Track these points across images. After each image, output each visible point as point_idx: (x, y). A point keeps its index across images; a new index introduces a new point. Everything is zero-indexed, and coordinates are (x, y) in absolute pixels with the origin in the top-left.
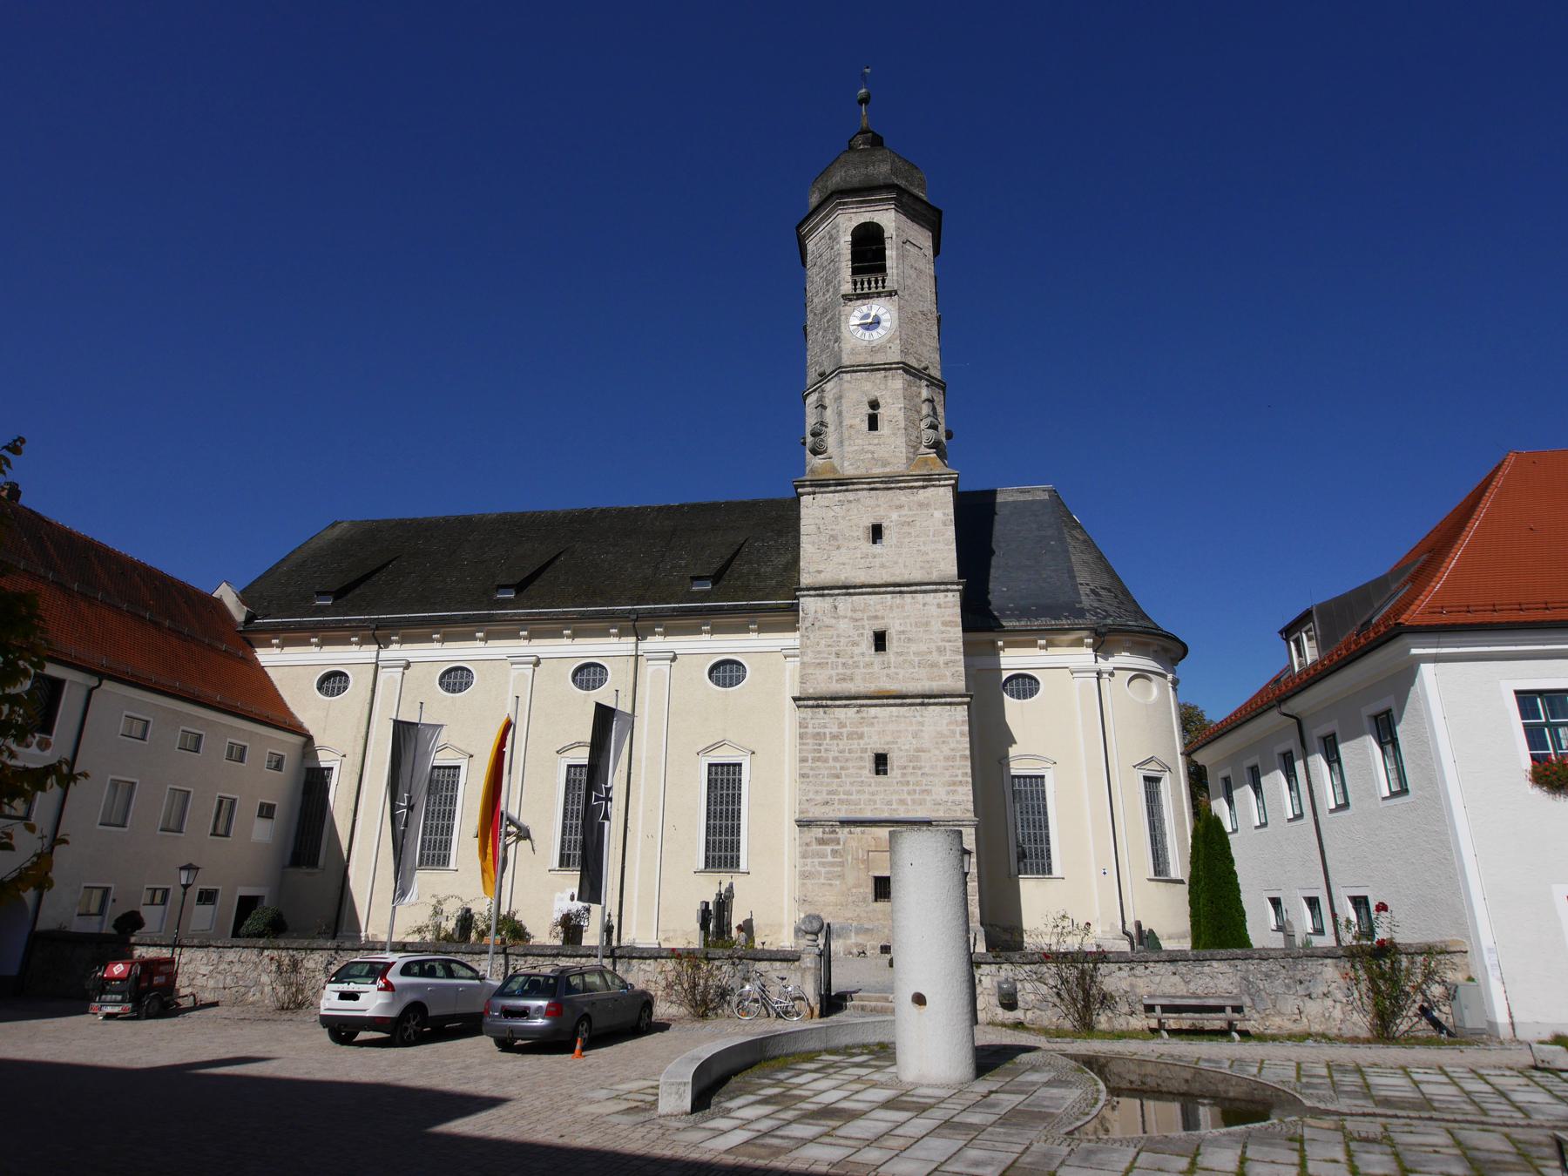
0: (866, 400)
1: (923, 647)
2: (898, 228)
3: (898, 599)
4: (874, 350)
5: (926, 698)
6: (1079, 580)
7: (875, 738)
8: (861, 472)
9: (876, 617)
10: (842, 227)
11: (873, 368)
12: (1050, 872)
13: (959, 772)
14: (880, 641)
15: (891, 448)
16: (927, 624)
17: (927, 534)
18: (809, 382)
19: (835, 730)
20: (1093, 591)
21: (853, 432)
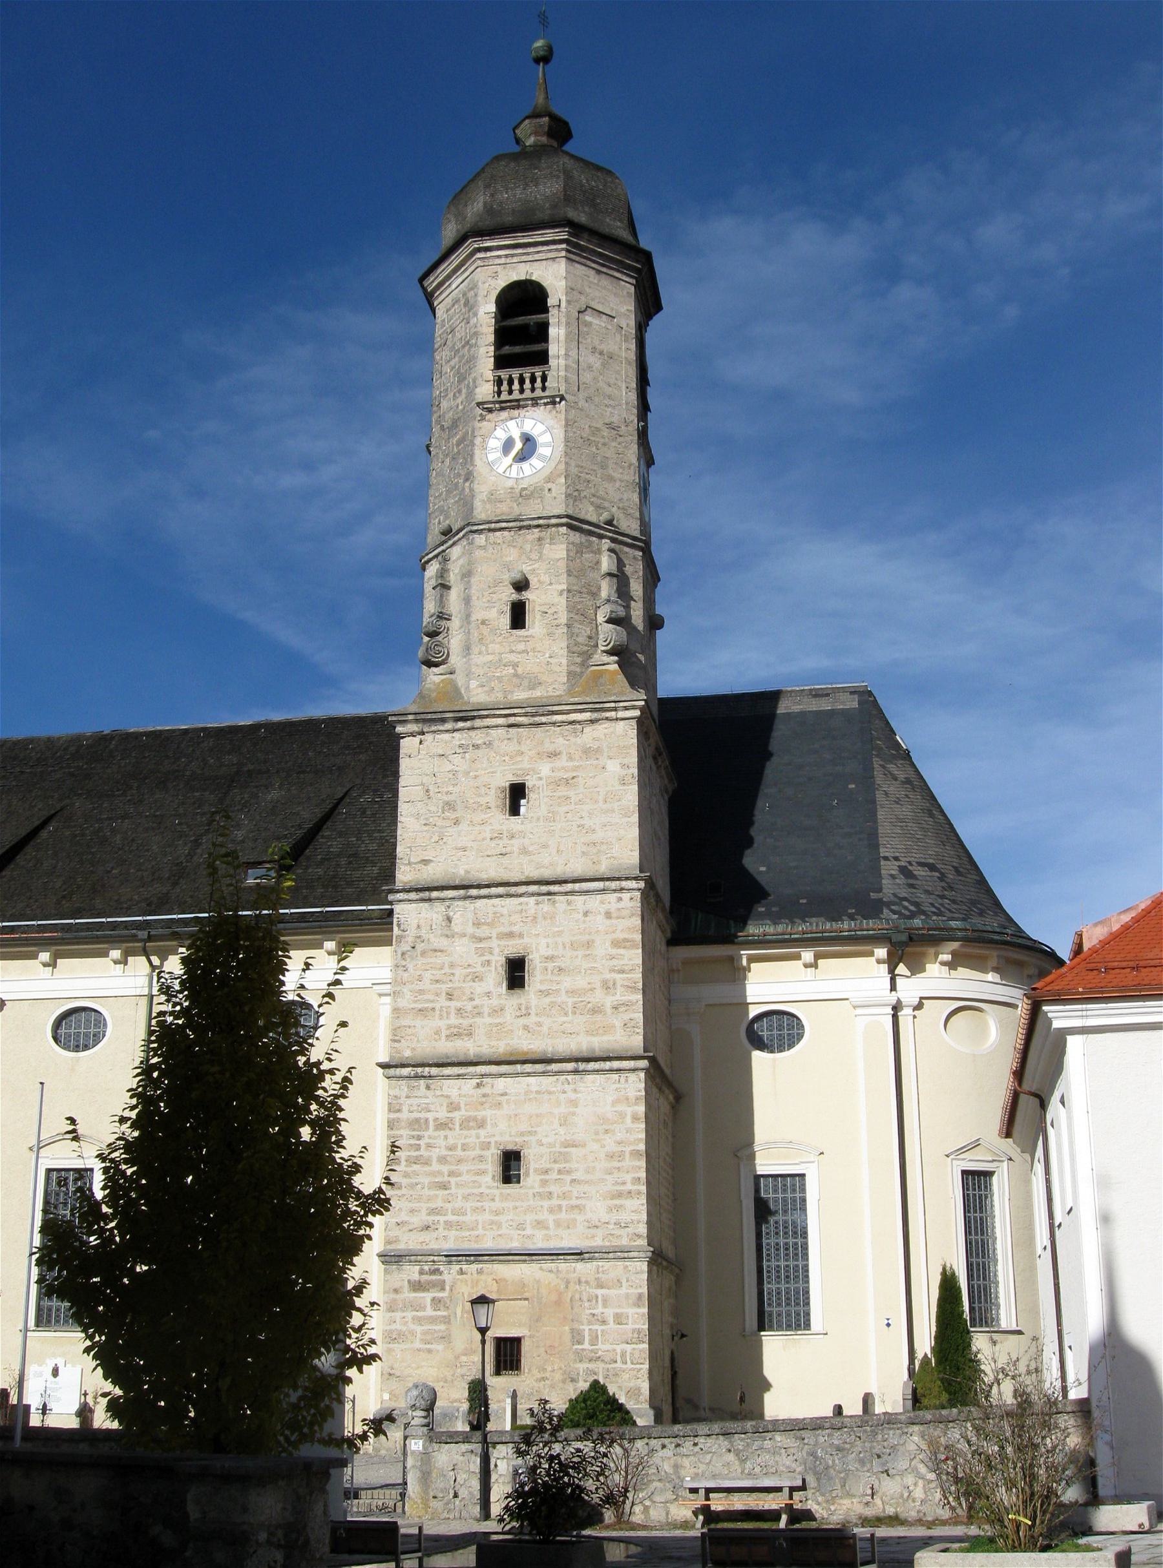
0: (507, 577)
1: (581, 982)
2: (570, 290)
3: (546, 906)
4: (525, 495)
5: (583, 1060)
6: (883, 852)
7: (503, 1126)
8: (497, 697)
9: (511, 935)
10: (482, 289)
11: (521, 525)
12: (808, 1326)
13: (628, 1177)
14: (516, 973)
15: (544, 657)
16: (589, 944)
17: (597, 799)
18: (429, 539)
19: (443, 1114)
20: (904, 871)
21: (485, 630)
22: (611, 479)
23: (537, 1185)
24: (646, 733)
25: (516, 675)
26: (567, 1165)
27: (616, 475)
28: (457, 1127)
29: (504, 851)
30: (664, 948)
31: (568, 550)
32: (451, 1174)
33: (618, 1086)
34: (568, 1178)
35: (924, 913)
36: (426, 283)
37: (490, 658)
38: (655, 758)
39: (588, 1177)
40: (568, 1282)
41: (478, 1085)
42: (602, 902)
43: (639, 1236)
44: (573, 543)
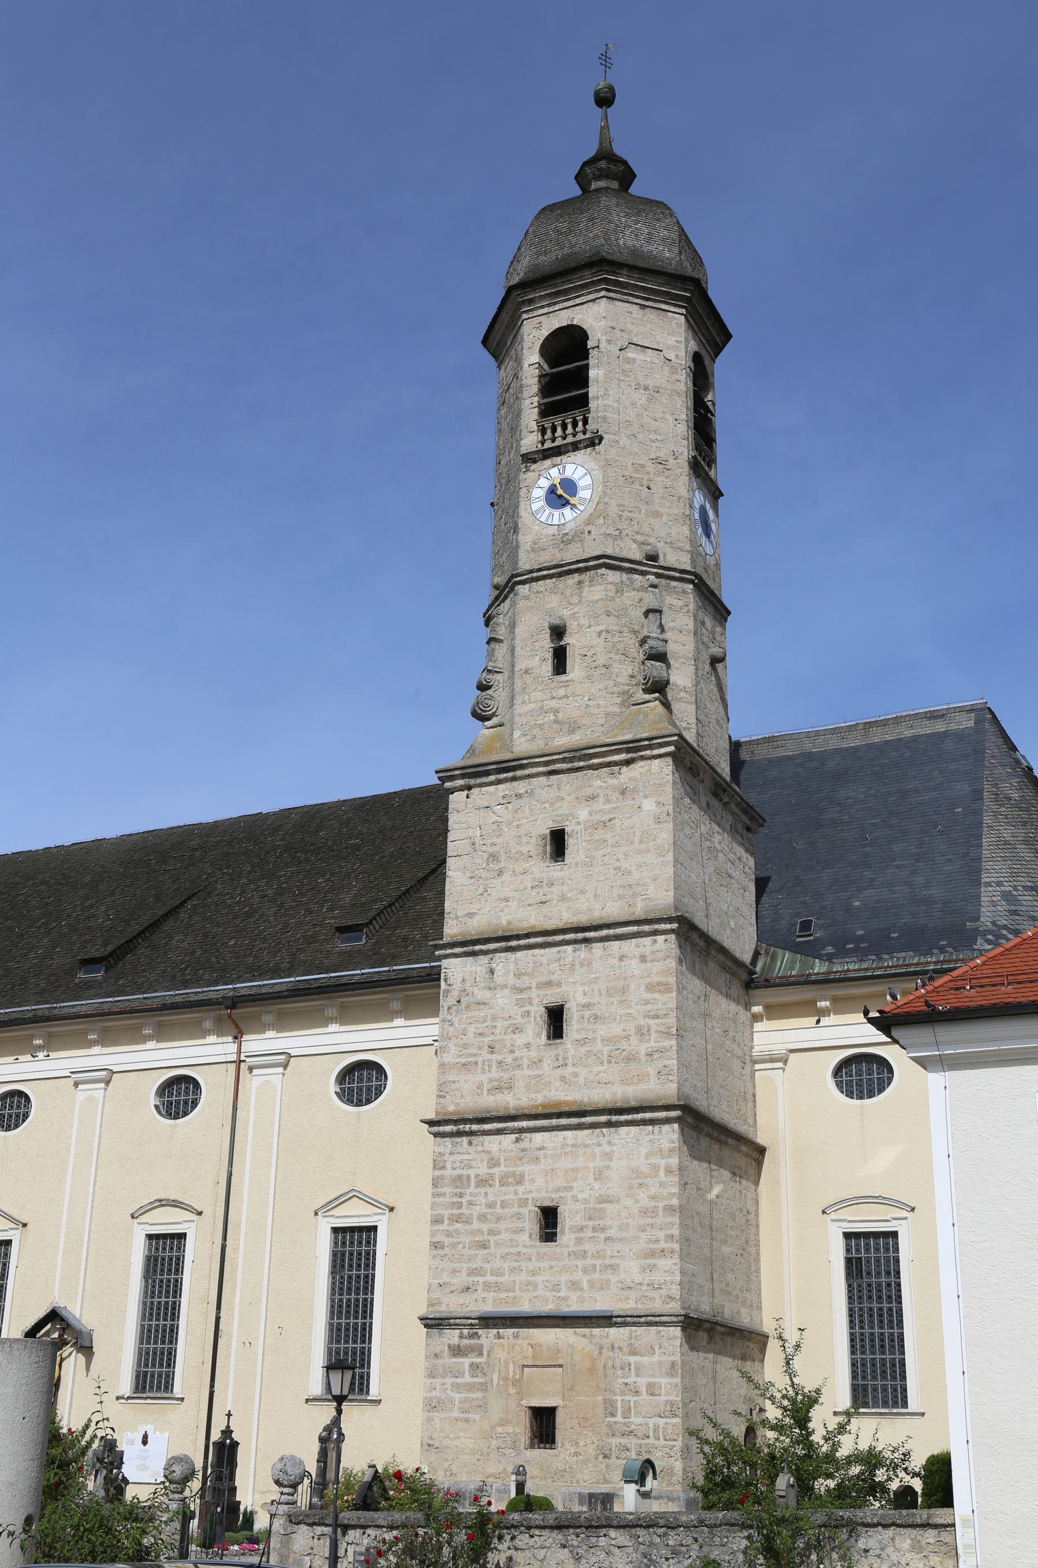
1: (616, 1030)
13: (661, 1235)
22: (657, 515)
24: (623, 792)
25: (556, 721)
26: (602, 1222)
28: (497, 1183)
33: (651, 1137)
34: (602, 1236)
42: (637, 946)
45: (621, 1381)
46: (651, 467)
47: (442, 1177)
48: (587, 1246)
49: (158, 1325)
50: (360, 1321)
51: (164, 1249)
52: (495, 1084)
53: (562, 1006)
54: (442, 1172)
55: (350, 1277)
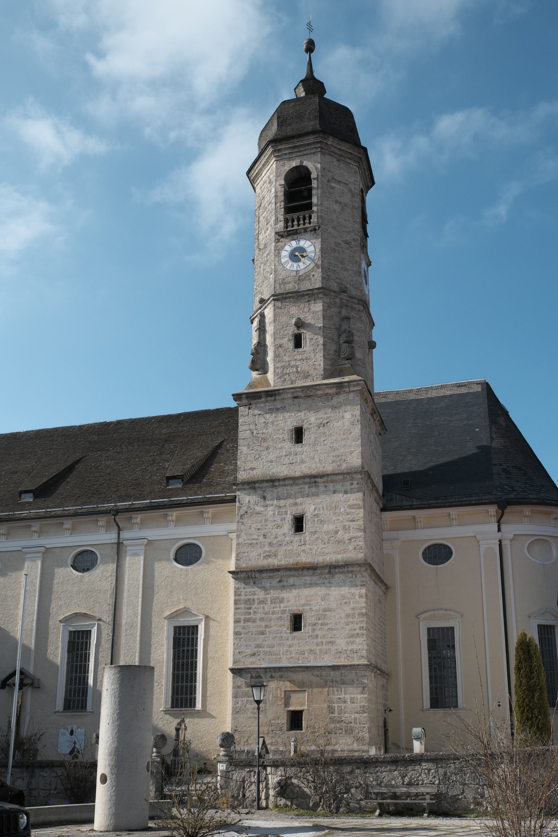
1: (332, 527)
4: (300, 278)
13: (357, 627)
20: (504, 470)
22: (346, 270)
23: (310, 631)
24: (366, 399)
26: (326, 621)
27: (349, 268)
28: (269, 603)
29: (292, 462)
30: (378, 512)
31: (323, 306)
32: (266, 627)
33: (351, 579)
34: (326, 628)
35: (515, 491)
36: (250, 175)
37: (284, 364)
38: (372, 415)
39: (336, 627)
40: (326, 681)
41: (280, 581)
42: (343, 486)
43: (363, 657)
44: (326, 302)
45: (337, 697)
46: (343, 245)
47: (240, 600)
48: (317, 632)
49: (76, 676)
50: (189, 672)
51: (78, 638)
52: (268, 554)
53: (303, 515)
54: (239, 597)
55: (183, 651)
